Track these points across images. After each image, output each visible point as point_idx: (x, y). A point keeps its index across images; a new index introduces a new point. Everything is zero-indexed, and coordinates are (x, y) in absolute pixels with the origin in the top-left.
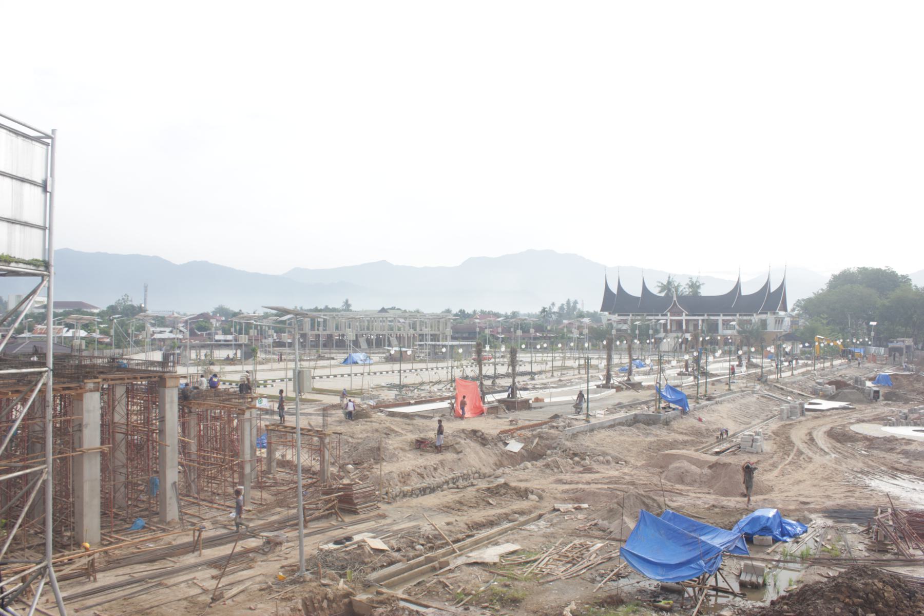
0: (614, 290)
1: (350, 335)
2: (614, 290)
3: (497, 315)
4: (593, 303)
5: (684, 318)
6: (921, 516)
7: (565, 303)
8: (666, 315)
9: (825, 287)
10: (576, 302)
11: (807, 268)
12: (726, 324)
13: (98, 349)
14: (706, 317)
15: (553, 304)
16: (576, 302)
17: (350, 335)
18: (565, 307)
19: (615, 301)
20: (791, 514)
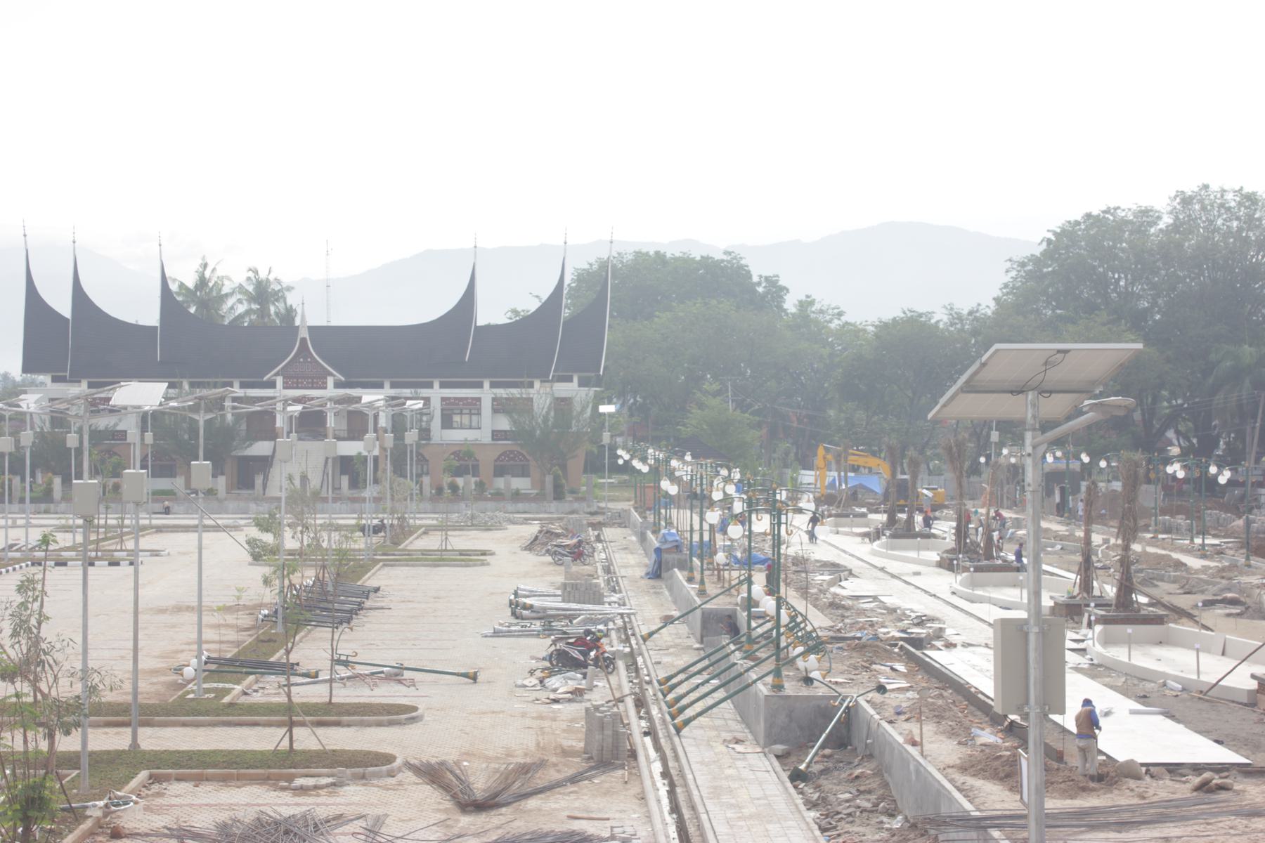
0: (64, 308)
2: (64, 308)
8: (272, 385)
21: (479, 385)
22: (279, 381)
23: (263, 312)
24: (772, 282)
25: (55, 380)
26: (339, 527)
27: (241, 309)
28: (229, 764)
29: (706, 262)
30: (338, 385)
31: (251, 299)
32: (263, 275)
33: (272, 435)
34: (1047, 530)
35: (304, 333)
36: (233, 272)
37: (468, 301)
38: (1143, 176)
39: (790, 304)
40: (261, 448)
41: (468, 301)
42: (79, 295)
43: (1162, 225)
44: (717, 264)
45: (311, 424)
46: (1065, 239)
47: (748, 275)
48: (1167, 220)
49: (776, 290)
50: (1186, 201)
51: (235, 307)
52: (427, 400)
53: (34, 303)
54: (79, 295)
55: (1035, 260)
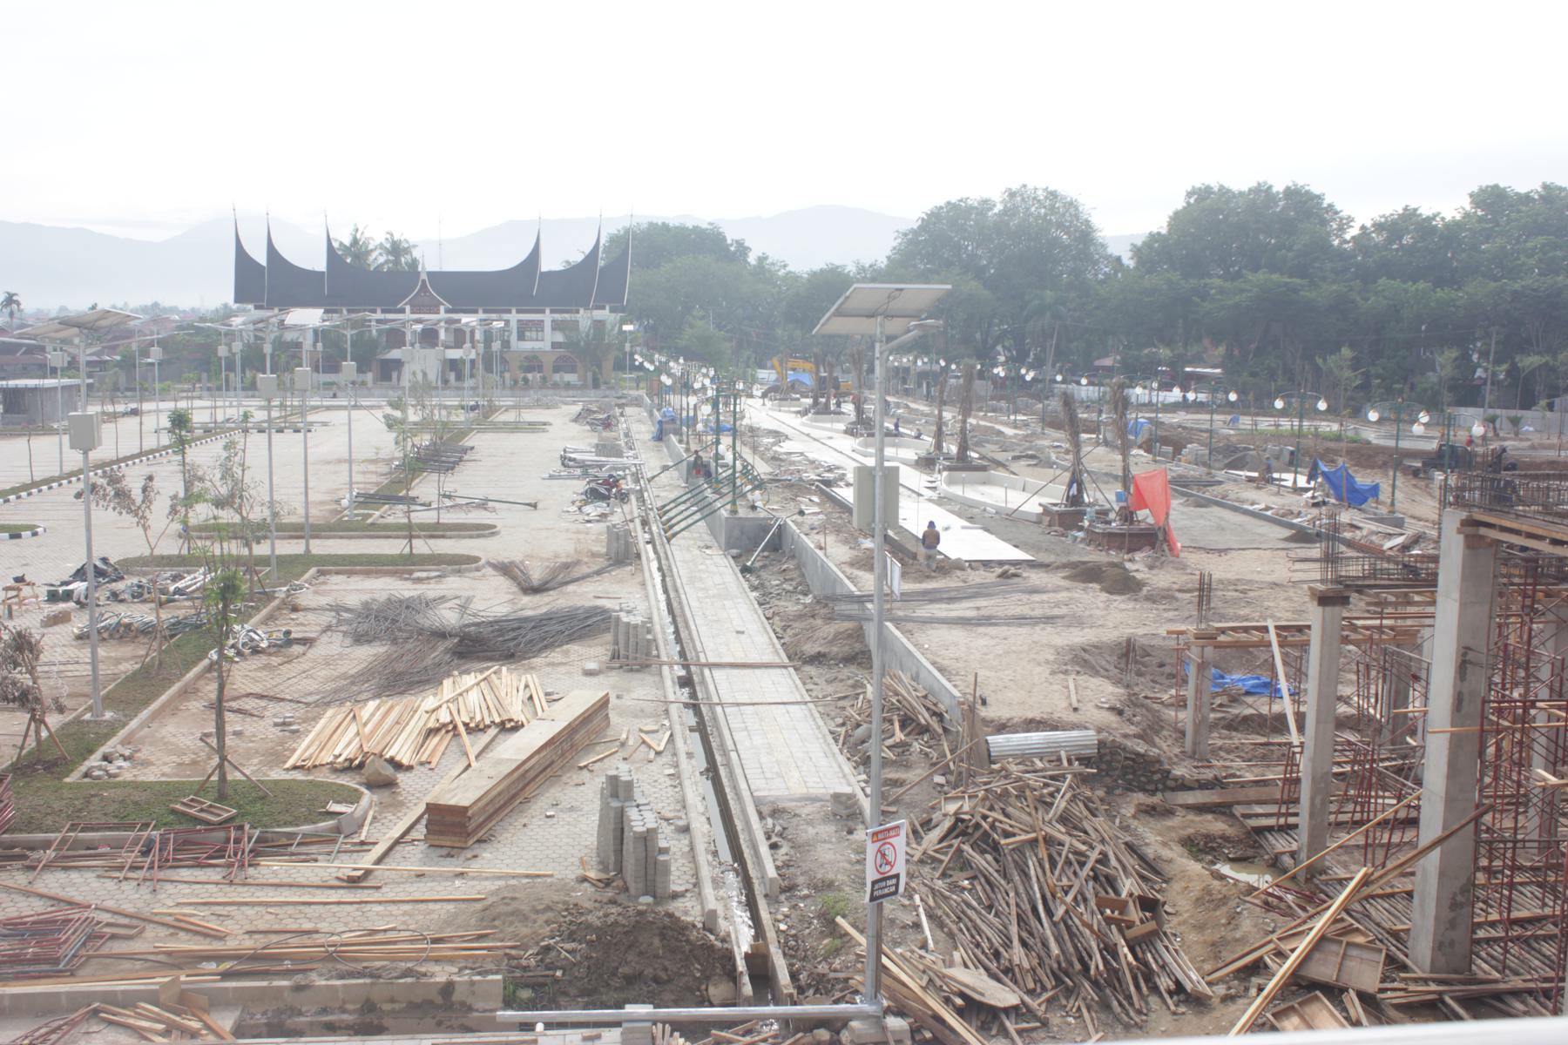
0: (261, 258)
2: (261, 258)
8: (402, 311)
19: (265, 280)
22: (408, 308)
23: (397, 262)
24: (740, 244)
27: (382, 260)
30: (448, 311)
31: (389, 252)
37: (535, 255)
39: (752, 259)
40: (395, 354)
41: (535, 255)
42: (272, 251)
43: (996, 210)
44: (703, 231)
45: (429, 337)
46: (934, 218)
47: (724, 239)
48: (999, 207)
49: (743, 249)
50: (1012, 195)
51: (378, 259)
52: (507, 322)
53: (243, 260)
54: (272, 251)
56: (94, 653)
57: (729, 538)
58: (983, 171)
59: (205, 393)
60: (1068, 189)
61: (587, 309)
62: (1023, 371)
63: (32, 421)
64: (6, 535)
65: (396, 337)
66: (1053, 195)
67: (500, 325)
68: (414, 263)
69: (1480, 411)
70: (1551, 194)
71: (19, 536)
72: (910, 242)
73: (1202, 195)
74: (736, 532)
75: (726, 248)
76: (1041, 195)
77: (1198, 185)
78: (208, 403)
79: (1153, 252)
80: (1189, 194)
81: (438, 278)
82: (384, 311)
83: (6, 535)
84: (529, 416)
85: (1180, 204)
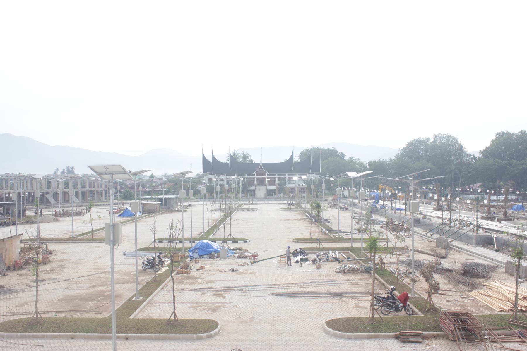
0: (210, 160)
1: (38, 193)
2: (210, 160)
3: (32, 179)
4: (198, 170)
5: (266, 176)
6: (3, 337)
7: (65, 169)
8: (254, 175)
9: (388, 160)
10: (73, 168)
11: (375, 138)
12: (290, 179)
13: (77, 193)
14: (246, 176)
15: (57, 170)
16: (73, 168)
17: (38, 193)
18: (66, 171)
19: (211, 166)
20: (217, 241)
21: (275, 175)
22: (256, 174)
23: (245, 160)
24: (342, 153)
25: (209, 174)
26: (226, 204)
27: (241, 160)
28: (416, 336)
29: (329, 150)
30: (268, 175)
31: (243, 157)
32: (245, 153)
33: (254, 185)
34: (358, 208)
35: (261, 164)
36: (240, 153)
37: (292, 157)
38: (515, 126)
39: (346, 158)
40: (253, 188)
41: (292, 157)
42: (213, 157)
43: (430, 141)
44: (331, 150)
45: (261, 182)
46: (410, 144)
47: (337, 152)
48: (432, 140)
49: (343, 155)
50: (436, 136)
51: (240, 160)
52: (244, 178)
53: (204, 160)
54: (213, 157)
55: (404, 149)
56: (37, 284)
57: (477, 241)
58: (427, 130)
59: (199, 200)
60: (454, 134)
61: (309, 174)
62: (397, 192)
63: (169, 208)
64: (243, 241)
65: (251, 182)
66: (449, 136)
67: (242, 179)
68: (252, 160)
69: (108, 208)
70: (523, 133)
71: (237, 242)
72: (403, 152)
73: (501, 135)
74: (479, 239)
75: (338, 155)
76: (445, 136)
77: (499, 131)
78: (202, 203)
79: (487, 153)
80: (497, 135)
81: (265, 165)
82: (248, 175)
83: (243, 241)
84: (252, 206)
85: (494, 138)
